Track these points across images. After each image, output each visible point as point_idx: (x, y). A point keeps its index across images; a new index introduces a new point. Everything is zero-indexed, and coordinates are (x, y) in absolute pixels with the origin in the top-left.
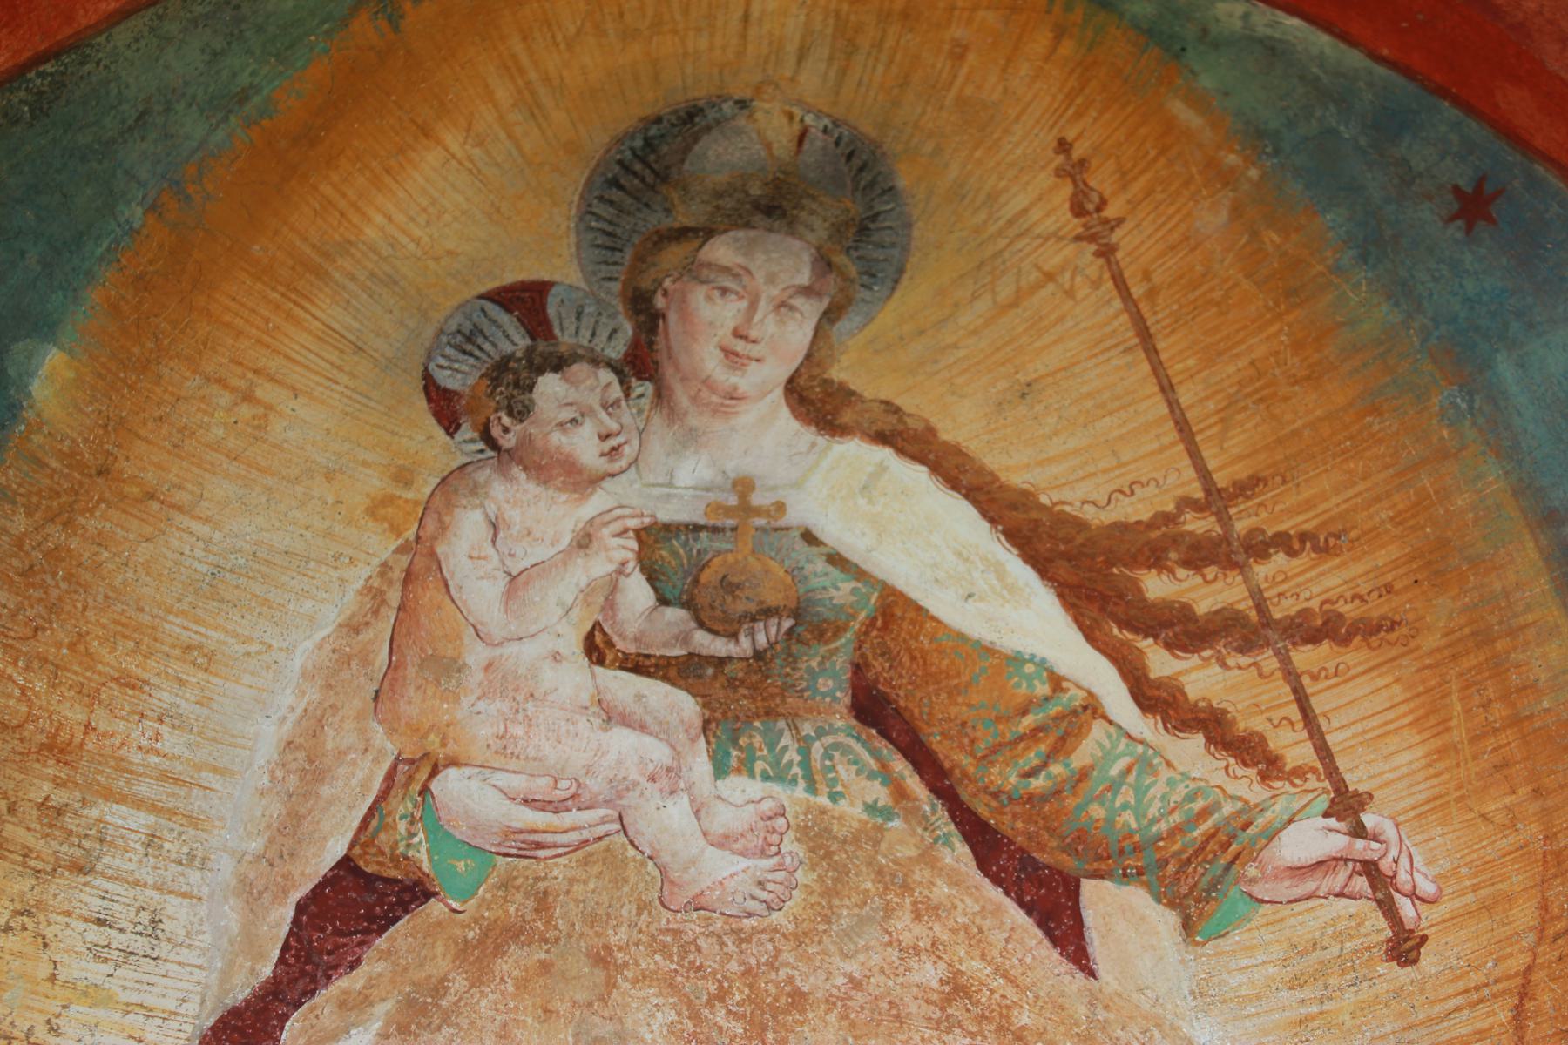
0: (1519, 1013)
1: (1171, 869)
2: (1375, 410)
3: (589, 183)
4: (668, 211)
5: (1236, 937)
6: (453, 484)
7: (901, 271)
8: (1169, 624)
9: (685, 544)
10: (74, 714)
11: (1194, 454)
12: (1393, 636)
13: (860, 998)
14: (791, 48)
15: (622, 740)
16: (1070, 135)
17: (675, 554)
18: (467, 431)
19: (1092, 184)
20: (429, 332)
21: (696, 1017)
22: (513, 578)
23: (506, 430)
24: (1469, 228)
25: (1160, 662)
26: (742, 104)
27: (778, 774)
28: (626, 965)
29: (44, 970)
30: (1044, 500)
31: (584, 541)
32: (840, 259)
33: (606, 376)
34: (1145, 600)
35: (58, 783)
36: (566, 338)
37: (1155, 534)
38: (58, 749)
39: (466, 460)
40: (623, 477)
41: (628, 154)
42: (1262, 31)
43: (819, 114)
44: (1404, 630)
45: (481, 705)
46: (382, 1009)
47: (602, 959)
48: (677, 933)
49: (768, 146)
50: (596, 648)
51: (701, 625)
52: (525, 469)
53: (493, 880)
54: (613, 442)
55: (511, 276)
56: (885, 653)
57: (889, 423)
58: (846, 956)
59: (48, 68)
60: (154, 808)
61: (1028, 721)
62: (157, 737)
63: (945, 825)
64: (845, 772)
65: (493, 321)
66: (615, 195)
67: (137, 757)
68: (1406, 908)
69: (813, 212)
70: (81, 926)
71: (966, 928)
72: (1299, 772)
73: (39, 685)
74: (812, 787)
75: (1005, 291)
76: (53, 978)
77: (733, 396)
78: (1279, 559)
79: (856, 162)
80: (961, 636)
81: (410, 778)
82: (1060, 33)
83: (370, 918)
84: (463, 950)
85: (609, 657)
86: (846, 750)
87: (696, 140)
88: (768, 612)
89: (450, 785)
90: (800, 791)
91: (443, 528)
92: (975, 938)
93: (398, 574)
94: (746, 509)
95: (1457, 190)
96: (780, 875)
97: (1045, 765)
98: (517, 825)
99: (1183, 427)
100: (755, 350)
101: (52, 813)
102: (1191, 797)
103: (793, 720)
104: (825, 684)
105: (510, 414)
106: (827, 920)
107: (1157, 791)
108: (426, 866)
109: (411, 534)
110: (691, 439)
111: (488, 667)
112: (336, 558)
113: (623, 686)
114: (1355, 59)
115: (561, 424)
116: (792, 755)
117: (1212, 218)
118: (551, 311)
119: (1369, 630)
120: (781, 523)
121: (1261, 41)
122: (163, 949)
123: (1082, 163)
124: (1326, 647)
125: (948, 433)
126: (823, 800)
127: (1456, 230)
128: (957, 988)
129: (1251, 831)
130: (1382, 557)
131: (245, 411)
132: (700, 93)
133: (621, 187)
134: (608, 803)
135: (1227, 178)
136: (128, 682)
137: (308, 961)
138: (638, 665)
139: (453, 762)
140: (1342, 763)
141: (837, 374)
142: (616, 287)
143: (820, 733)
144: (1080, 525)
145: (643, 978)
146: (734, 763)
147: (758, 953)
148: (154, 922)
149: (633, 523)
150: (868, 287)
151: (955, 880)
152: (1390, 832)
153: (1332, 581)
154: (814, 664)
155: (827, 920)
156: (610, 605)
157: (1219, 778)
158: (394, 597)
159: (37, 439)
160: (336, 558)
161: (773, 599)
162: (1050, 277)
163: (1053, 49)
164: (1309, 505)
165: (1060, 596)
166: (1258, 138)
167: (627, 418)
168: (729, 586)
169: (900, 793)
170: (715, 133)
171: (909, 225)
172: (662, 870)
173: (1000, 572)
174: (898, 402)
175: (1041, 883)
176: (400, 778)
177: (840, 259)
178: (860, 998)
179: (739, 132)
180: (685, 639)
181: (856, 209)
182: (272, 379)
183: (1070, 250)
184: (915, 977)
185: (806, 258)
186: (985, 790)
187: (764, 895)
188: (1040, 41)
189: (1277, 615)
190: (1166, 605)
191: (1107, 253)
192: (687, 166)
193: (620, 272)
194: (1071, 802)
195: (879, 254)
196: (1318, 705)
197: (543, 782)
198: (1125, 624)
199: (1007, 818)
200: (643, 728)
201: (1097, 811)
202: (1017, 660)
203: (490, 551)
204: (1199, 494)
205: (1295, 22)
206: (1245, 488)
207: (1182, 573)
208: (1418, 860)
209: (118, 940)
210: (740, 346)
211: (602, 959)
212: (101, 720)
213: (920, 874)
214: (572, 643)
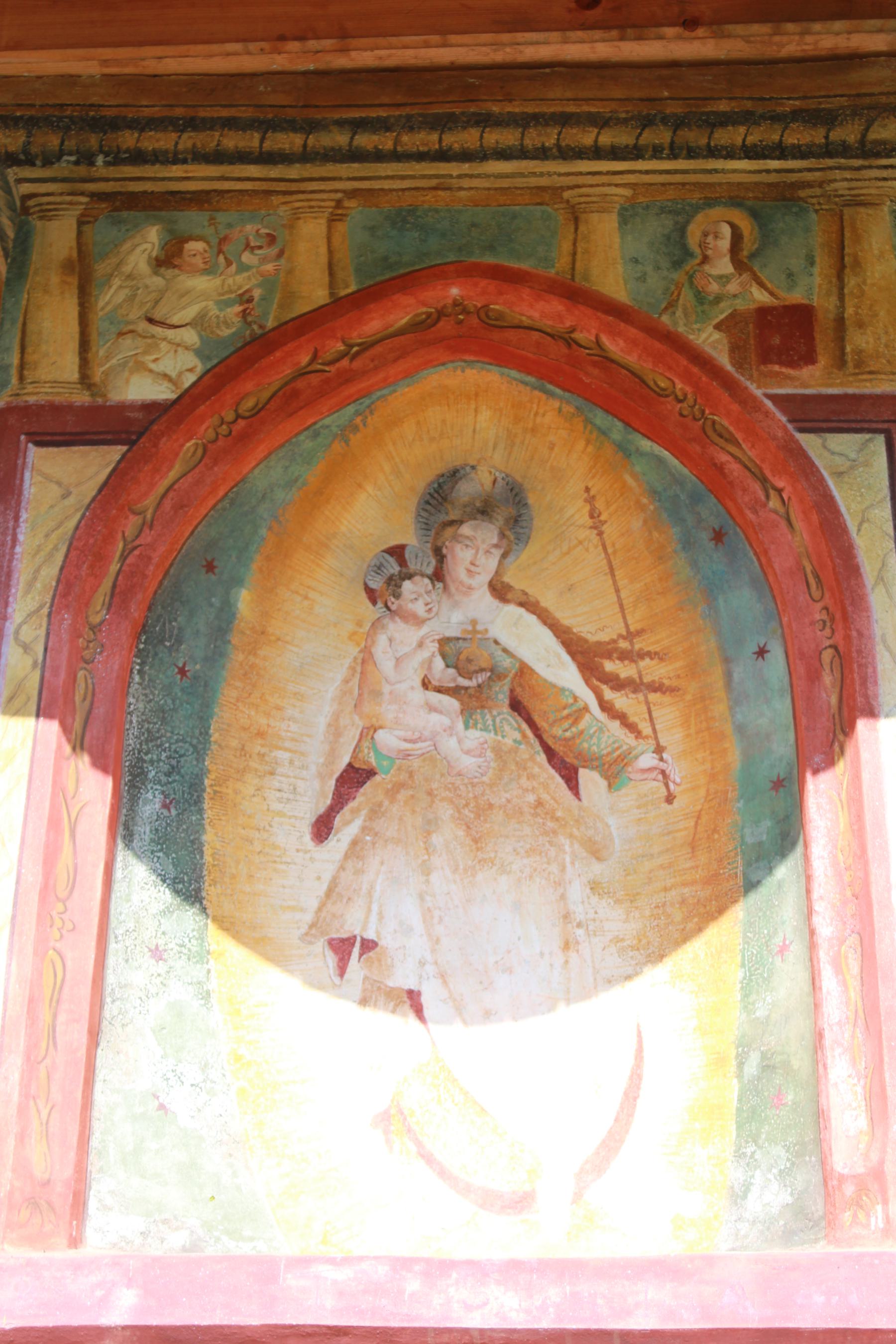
0: (696, 823)
1: (606, 766)
2: (681, 609)
3: (419, 503)
4: (447, 513)
5: (623, 791)
6: (376, 625)
7: (529, 538)
8: (611, 681)
9: (454, 645)
10: (263, 721)
11: (624, 617)
12: (677, 693)
13: (509, 806)
14: (491, 444)
15: (435, 717)
16: (590, 485)
17: (451, 648)
18: (380, 604)
19: (597, 506)
20: (365, 566)
21: (459, 812)
22: (397, 659)
23: (393, 603)
24: (716, 545)
26: (473, 467)
27: (485, 729)
28: (437, 795)
29: (265, 807)
30: (575, 630)
31: (420, 645)
32: (508, 533)
33: (427, 581)
34: (604, 671)
35: (262, 746)
36: (413, 566)
37: (610, 647)
38: (261, 734)
39: (379, 615)
40: (432, 620)
41: (432, 491)
42: (657, 453)
43: (501, 472)
44: (681, 692)
45: (389, 707)
46: (364, 813)
47: (430, 793)
48: (453, 784)
49: (482, 485)
50: (426, 684)
51: (460, 675)
52: (400, 618)
53: (395, 767)
54: (429, 606)
55: (393, 543)
56: (521, 685)
57: (523, 599)
58: (506, 792)
59: (235, 490)
60: (290, 750)
61: (566, 712)
62: (289, 726)
63: (538, 748)
64: (507, 728)
65: (387, 561)
66: (428, 507)
67: (283, 734)
68: (672, 786)
69: (498, 514)
70: (274, 792)
71: (543, 783)
72: (647, 737)
73: (253, 713)
74: (496, 734)
75: (565, 548)
76: (268, 810)
77: (470, 588)
78: (647, 660)
79: (514, 492)
80: (545, 681)
81: (367, 734)
82: (588, 442)
83: (358, 782)
84: (387, 792)
85: (430, 687)
86: (507, 720)
87: (456, 483)
88: (482, 670)
89: (381, 735)
90: (492, 735)
91: (373, 642)
92: (546, 787)
93: (359, 661)
94: (475, 631)
95: (714, 530)
96: (485, 764)
97: (570, 728)
98: (402, 748)
99: (621, 606)
100: (477, 570)
101: (262, 756)
102: (614, 742)
103: (490, 709)
104: (501, 696)
105: (394, 596)
106: (500, 779)
107: (604, 739)
108: (374, 764)
109: (363, 645)
110: (456, 605)
111: (391, 693)
112: (340, 655)
113: (435, 698)
114: (685, 471)
115: (411, 601)
116: (490, 722)
117: (637, 524)
118: (407, 556)
119: (672, 690)
120: (487, 636)
121: (656, 456)
122: (298, 797)
123: (593, 497)
124: (658, 695)
125: (544, 603)
126: (499, 738)
127: (712, 544)
128: (539, 803)
129: (631, 755)
130: (679, 664)
131: (306, 603)
132: (458, 463)
133: (430, 504)
134: (431, 740)
135: (642, 508)
136: (279, 708)
137: (341, 798)
138: (439, 690)
139: (381, 727)
140: (659, 735)
141: (506, 579)
142: (429, 545)
143: (499, 714)
144: (586, 641)
145: (443, 799)
146: (471, 725)
147: (479, 790)
148: (295, 789)
149: (437, 637)
150: (517, 544)
151: (540, 766)
152: (670, 761)
153: (662, 671)
154: (497, 689)
155: (500, 779)
156: (430, 668)
157: (623, 737)
158: (359, 669)
159: (242, 624)
160: (340, 655)
161: (484, 665)
162: (581, 543)
163: (585, 448)
164: (657, 642)
165: (579, 667)
166: (654, 493)
167: (434, 597)
168: (469, 661)
169: (524, 736)
170: (463, 480)
171: (532, 519)
172: (448, 762)
173: (559, 657)
174: (527, 590)
175: (567, 769)
176: (364, 734)
177: (508, 533)
178: (509, 806)
179: (472, 480)
180: (454, 680)
181: (514, 512)
182: (314, 590)
183: (588, 532)
184: (527, 799)
185: (496, 532)
186: (551, 736)
187: (480, 771)
188: (581, 445)
189: (645, 681)
190: (611, 674)
191: (600, 534)
192: (453, 495)
193: (430, 539)
194: (578, 741)
195: (521, 531)
196: (654, 714)
197: (410, 733)
198: (599, 680)
199: (557, 746)
200: (441, 712)
201: (585, 745)
202: (563, 690)
203: (389, 649)
204: (624, 633)
205: (666, 453)
206: (639, 633)
207: (617, 662)
208: (677, 771)
209: (285, 795)
210: (472, 568)
211: (430, 793)
212: (272, 722)
213: (529, 764)
214: (418, 683)
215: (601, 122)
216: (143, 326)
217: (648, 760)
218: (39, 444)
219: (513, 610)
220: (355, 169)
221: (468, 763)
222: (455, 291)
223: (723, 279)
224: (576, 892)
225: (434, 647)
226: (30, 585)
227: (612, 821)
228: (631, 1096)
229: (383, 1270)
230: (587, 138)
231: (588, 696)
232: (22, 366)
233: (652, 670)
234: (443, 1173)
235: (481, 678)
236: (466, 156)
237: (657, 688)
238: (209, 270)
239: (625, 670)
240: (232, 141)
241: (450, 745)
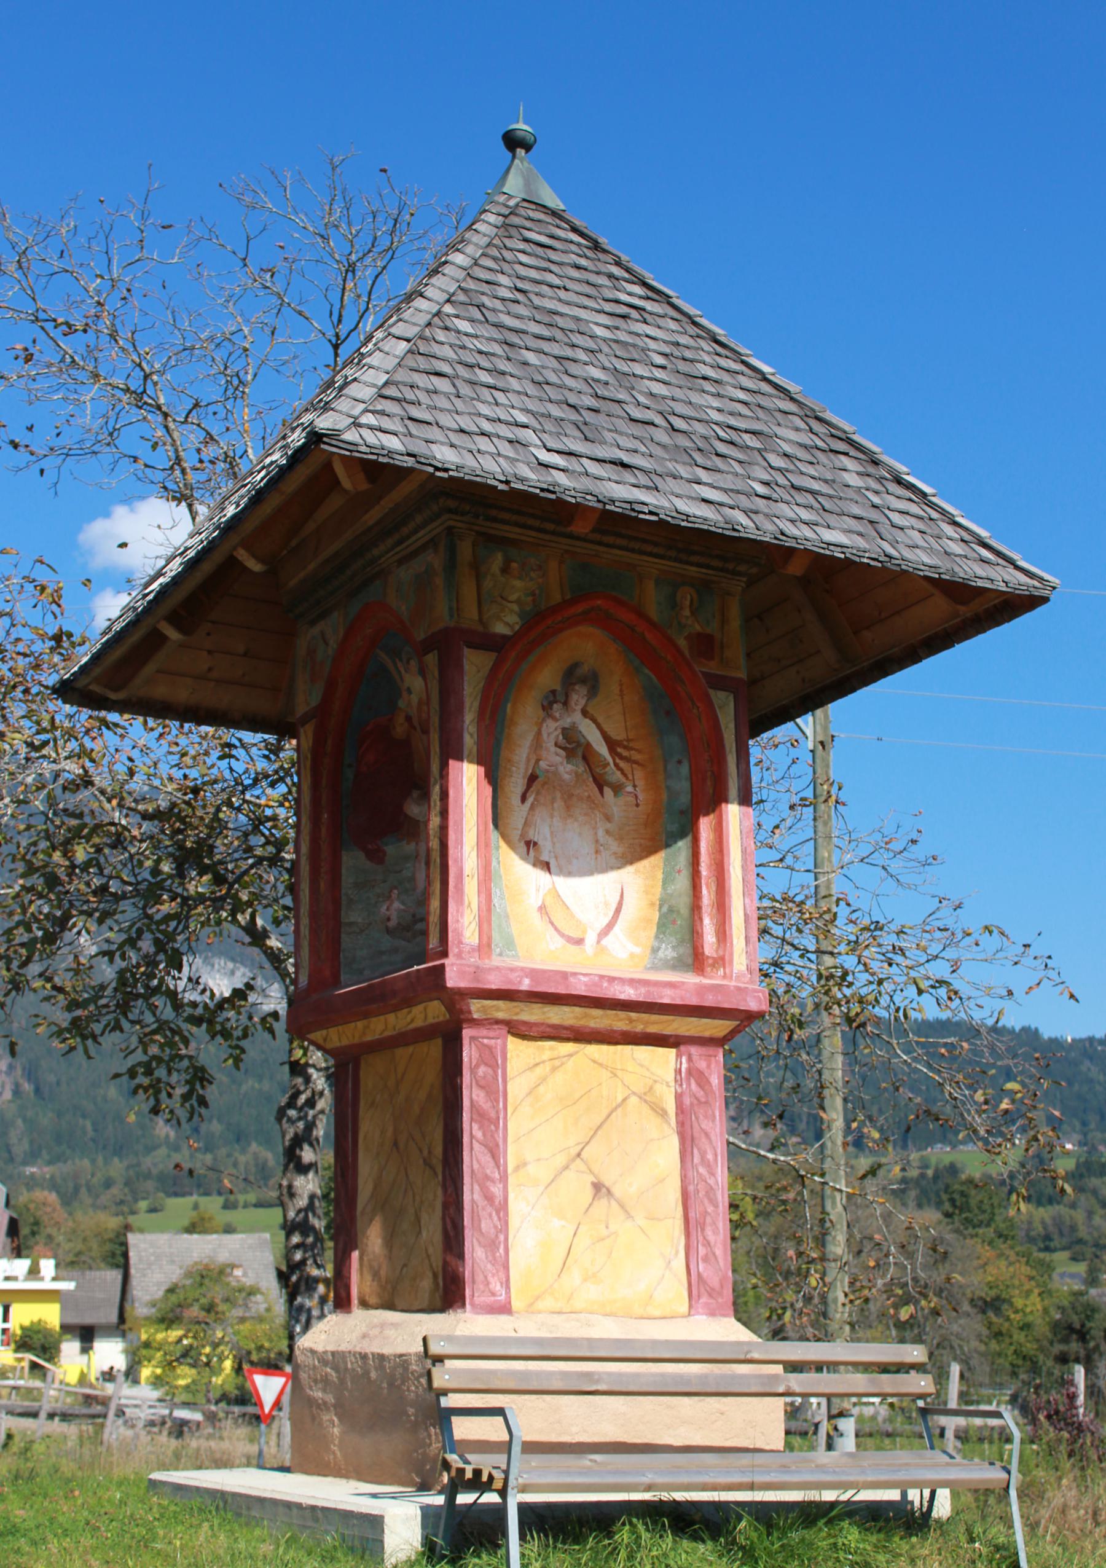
6: (544, 720)
25: (618, 761)
36: (558, 698)
50: (556, 745)
110: (569, 716)
138: (560, 747)
206: (632, 740)
215: (655, 544)
216: (499, 599)
217: (630, 789)
218: (469, 647)
219: (588, 721)
220: (569, 541)
221: (566, 777)
222: (599, 602)
223: (687, 617)
224: (601, 833)
225: (559, 731)
226: (471, 707)
227: (615, 809)
228: (618, 910)
229: (597, 978)
230: (649, 548)
231: (610, 759)
232: (458, 609)
233: (636, 756)
234: (556, 929)
235: (574, 745)
236: (608, 545)
237: (636, 762)
238: (520, 578)
239: (625, 753)
240: (531, 522)
241: (561, 769)
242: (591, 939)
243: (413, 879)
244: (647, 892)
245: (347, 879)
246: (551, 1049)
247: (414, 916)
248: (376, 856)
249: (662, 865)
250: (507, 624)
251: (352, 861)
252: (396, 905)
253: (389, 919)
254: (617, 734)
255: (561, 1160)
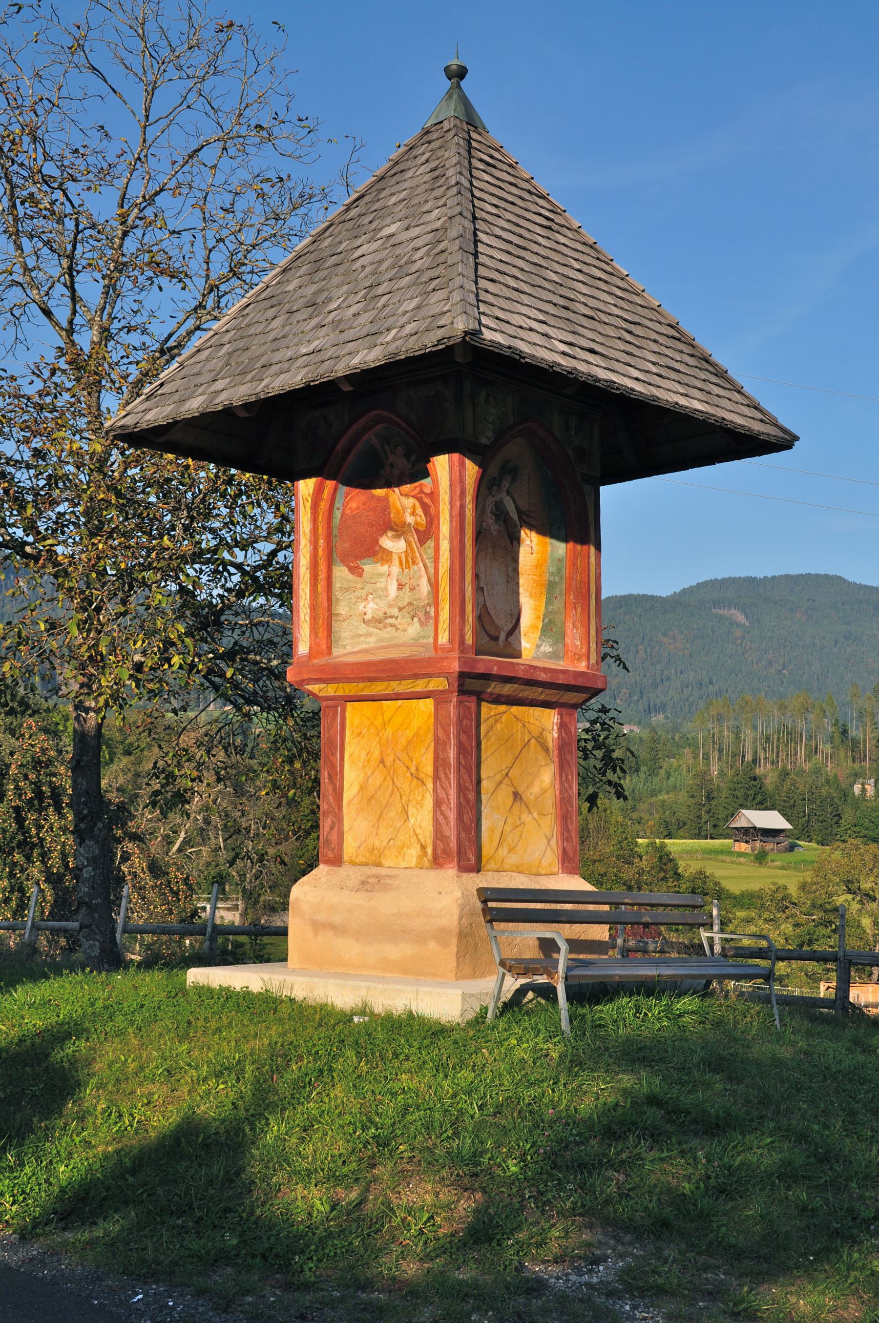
50: (491, 513)
219: (509, 498)
239: (527, 520)
242: (503, 636)
243: (385, 589)
244: (536, 609)
245: (337, 584)
246: (495, 709)
247: (385, 613)
248: (357, 571)
249: (545, 593)
250: (487, 437)
251: (341, 572)
252: (371, 605)
253: (365, 614)
254: (524, 507)
255: (498, 777)
